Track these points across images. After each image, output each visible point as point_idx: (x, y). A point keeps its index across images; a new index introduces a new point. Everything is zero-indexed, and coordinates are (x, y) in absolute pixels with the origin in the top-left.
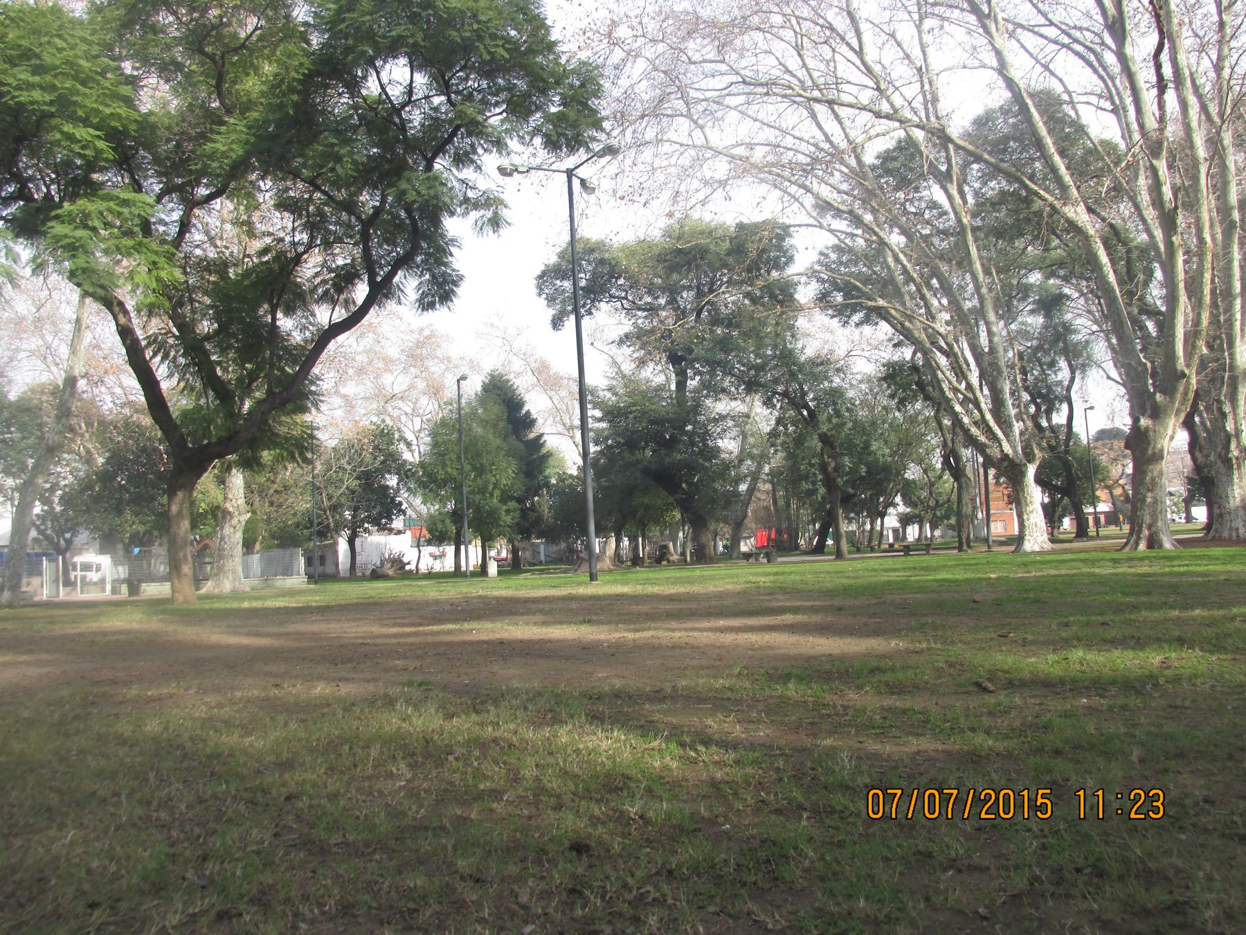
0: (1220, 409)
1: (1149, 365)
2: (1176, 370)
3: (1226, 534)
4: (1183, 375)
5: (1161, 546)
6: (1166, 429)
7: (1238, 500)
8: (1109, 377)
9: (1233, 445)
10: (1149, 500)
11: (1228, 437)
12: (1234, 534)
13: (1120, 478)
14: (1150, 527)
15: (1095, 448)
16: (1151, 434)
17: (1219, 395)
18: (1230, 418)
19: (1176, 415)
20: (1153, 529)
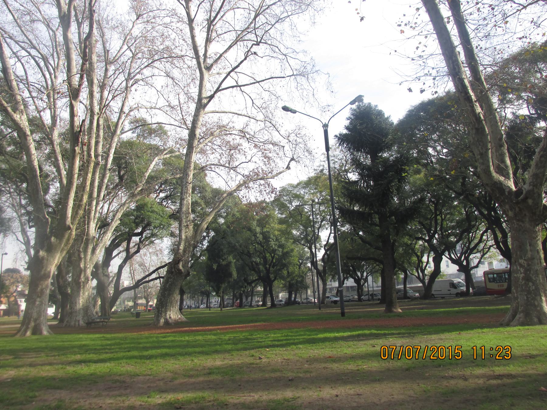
0: (79, 255)
1: (50, 220)
2: (65, 224)
3: (73, 323)
4: (69, 228)
5: (41, 333)
6: (54, 260)
7: (81, 305)
8: (18, 239)
9: (82, 276)
10: (37, 303)
11: (81, 271)
12: (77, 324)
13: (14, 292)
14: (35, 320)
15: (3, 276)
16: (45, 261)
17: (80, 247)
18: (83, 260)
19: (61, 252)
20: (38, 322)
